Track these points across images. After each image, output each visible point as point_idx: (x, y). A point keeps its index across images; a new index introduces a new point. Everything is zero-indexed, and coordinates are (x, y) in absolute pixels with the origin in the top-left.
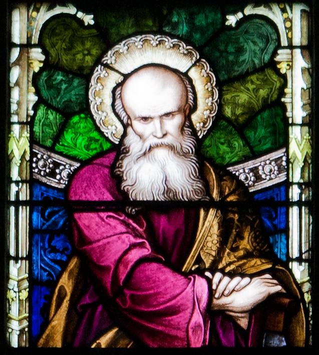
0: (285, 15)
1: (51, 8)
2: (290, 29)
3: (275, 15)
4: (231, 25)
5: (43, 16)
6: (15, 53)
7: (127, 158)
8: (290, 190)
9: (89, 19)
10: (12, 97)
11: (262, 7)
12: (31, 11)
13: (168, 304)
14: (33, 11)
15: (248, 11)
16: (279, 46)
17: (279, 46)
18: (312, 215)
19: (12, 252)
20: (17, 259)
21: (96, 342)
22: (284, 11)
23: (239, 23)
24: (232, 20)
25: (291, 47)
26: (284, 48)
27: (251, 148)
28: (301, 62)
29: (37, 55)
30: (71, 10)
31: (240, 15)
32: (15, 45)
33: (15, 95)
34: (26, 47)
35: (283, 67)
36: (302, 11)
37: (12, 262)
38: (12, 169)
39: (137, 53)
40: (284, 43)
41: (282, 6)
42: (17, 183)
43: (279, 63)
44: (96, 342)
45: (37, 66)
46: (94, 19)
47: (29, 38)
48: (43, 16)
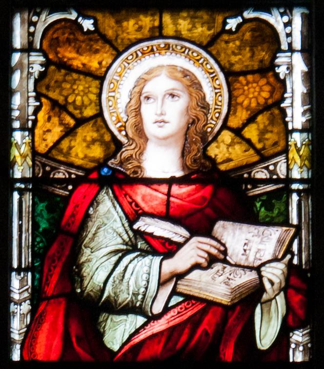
3: (276, 19)
4: (231, 29)
5: (46, 19)
6: (16, 57)
7: (293, 170)
8: (290, 200)
10: (13, 102)
12: (31, 14)
13: (132, 343)
14: (33, 15)
15: (249, 14)
16: (280, 50)
17: (280, 50)
18: (113, 306)
19: (15, 265)
20: (19, 270)
21: (297, 255)
23: (239, 26)
25: (291, 49)
26: (284, 51)
27: (258, 152)
28: (299, 64)
29: (37, 59)
31: (239, 20)
32: (16, 50)
33: (17, 100)
35: (282, 71)
36: (303, 15)
37: (14, 274)
38: (148, 177)
39: (209, 85)
40: (284, 46)
43: (279, 66)
44: (297, 255)
45: (37, 69)
47: (31, 43)
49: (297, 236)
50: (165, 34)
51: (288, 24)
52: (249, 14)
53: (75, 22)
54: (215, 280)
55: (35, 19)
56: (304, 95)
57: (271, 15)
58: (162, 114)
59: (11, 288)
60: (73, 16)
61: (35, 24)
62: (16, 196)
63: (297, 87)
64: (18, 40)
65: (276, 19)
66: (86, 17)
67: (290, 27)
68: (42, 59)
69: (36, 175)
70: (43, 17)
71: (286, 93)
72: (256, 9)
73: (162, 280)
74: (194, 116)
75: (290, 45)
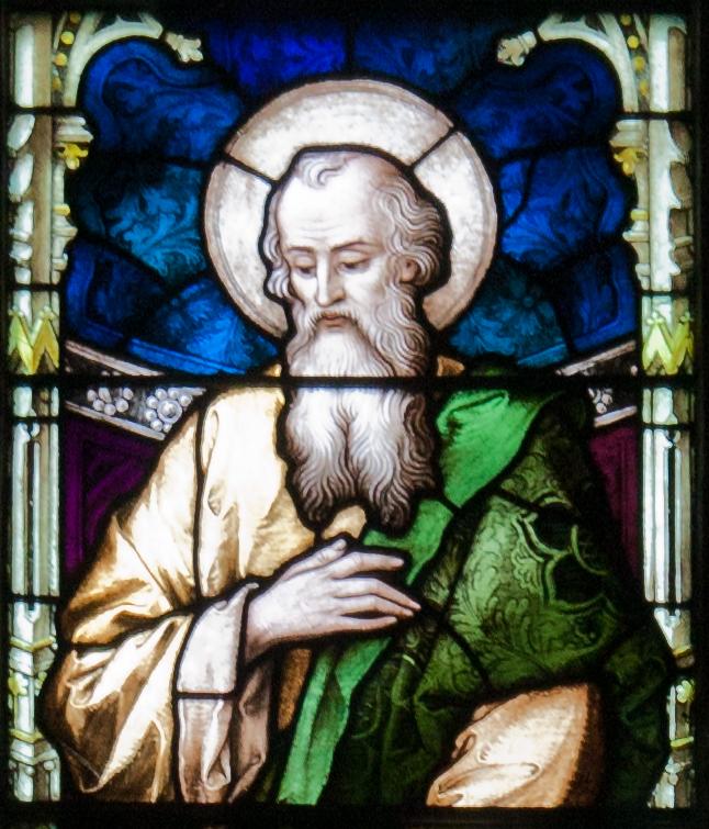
0: (633, 41)
1: (105, 22)
2: (642, 74)
3: (610, 42)
5: (88, 42)
9: (188, 50)
11: (581, 24)
12: (60, 27)
15: (553, 30)
16: (622, 114)
17: (622, 114)
19: (19, 586)
20: (30, 599)
22: (628, 31)
24: (515, 50)
28: (667, 150)
30: (151, 29)
33: (24, 225)
34: (52, 112)
37: (20, 607)
41: (626, 21)
42: (29, 421)
43: (620, 150)
46: (203, 49)
47: (57, 94)
48: (88, 42)
49: (385, 637)
50: (423, 507)
51: (641, 51)
52: (553, 30)
53: (160, 45)
54: (481, 453)
55: (68, 38)
56: (673, 213)
57: (601, 33)
58: (339, 300)
59: (114, 528)
60: (151, 29)
61: (66, 49)
62: (21, 436)
63: (662, 194)
64: (27, 92)
65: (610, 42)
66: (532, 57)
67: (651, 66)
68: (88, 137)
69: (13, 367)
70: (83, 34)
71: (636, 207)
72: (570, 15)
73: (249, 656)
74: (422, 475)
75: (643, 101)
